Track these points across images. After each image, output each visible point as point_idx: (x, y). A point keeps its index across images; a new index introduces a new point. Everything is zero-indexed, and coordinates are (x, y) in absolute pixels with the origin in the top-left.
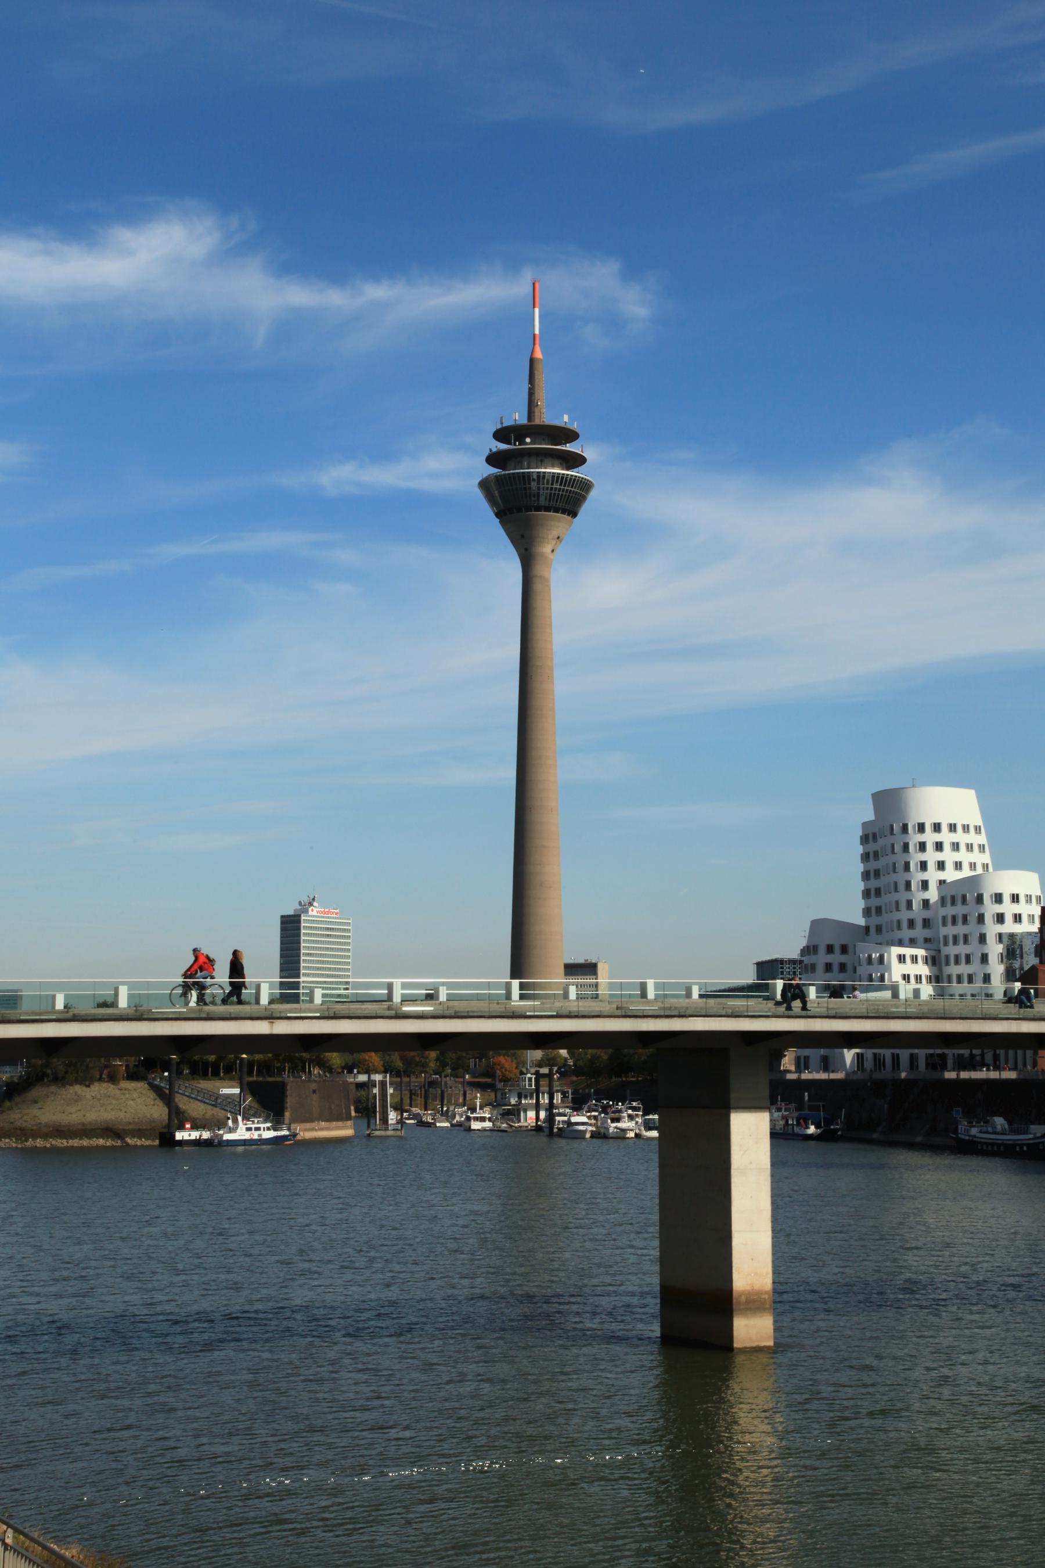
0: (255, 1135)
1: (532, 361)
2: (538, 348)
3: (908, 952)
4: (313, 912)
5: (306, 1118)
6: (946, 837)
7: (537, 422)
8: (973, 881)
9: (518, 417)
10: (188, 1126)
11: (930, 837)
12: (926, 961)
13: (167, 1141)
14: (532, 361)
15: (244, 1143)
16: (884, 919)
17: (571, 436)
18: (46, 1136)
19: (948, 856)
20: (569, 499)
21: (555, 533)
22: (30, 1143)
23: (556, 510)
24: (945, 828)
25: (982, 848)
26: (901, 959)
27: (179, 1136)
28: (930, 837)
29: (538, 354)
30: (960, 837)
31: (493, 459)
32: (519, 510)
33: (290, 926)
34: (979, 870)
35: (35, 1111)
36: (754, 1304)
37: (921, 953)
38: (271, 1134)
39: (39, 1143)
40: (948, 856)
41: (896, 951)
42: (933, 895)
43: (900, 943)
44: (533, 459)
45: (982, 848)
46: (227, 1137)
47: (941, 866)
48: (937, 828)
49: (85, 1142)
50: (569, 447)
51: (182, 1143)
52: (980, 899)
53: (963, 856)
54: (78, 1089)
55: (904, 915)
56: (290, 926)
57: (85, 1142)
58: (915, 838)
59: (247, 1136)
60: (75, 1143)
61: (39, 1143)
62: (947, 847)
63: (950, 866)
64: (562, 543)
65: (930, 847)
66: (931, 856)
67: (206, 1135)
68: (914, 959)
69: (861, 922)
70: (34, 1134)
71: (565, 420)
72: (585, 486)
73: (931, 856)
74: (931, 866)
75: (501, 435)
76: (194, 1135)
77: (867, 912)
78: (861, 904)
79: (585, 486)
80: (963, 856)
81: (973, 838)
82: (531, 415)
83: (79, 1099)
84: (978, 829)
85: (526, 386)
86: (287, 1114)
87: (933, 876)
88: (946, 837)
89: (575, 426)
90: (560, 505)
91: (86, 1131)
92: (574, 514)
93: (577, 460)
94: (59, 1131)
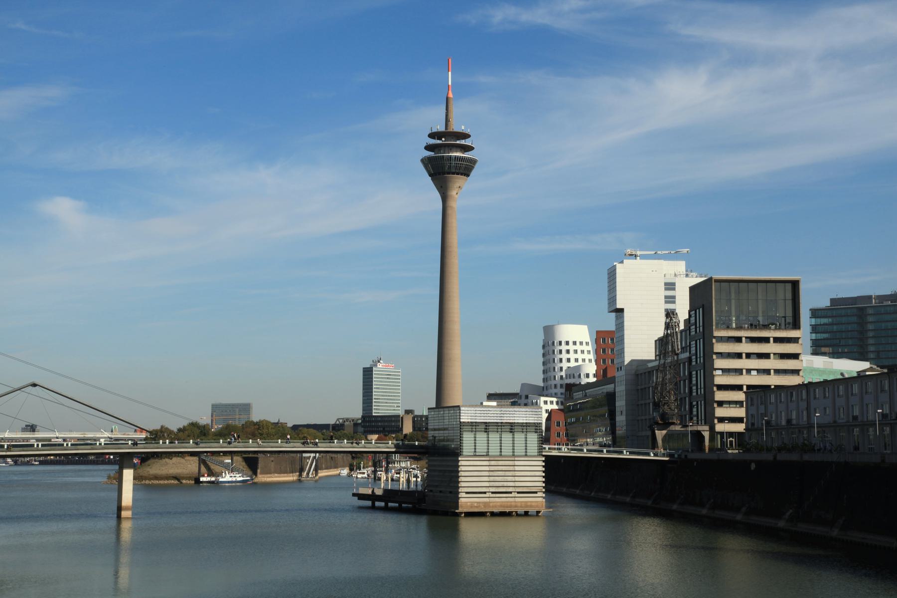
0: (234, 479)
1: (447, 98)
2: (450, 92)
3: (549, 399)
4: (380, 366)
5: (267, 472)
6: (571, 347)
7: (450, 130)
8: (578, 368)
9: (441, 128)
10: (753, 466)
11: (564, 347)
12: (557, 403)
13: (197, 481)
14: (447, 98)
15: (229, 482)
16: (549, 383)
17: (466, 136)
18: (150, 479)
19: (572, 356)
20: (466, 168)
21: (457, 185)
22: (143, 482)
23: (458, 174)
24: (578, 343)
25: (589, 352)
26: (546, 402)
27: (202, 479)
28: (564, 347)
29: (451, 95)
30: (578, 347)
31: (429, 148)
32: (439, 174)
33: (368, 373)
34: (580, 362)
35: (148, 469)
36: (127, 509)
37: (555, 400)
38: (241, 479)
39: (147, 482)
40: (572, 356)
41: (543, 399)
42: (563, 374)
43: (547, 396)
44: (447, 149)
45: (589, 352)
46: (221, 480)
47: (569, 360)
48: (575, 343)
49: (166, 482)
50: (463, 142)
51: (202, 482)
52: (580, 376)
53: (580, 356)
54: (167, 460)
55: (553, 383)
56: (368, 373)
57: (166, 482)
58: (558, 348)
59: (230, 479)
60: (162, 482)
61: (147, 482)
62: (579, 352)
63: (572, 360)
64: (463, 190)
65: (564, 352)
66: (564, 356)
67: (213, 479)
68: (552, 403)
69: (542, 384)
70: (146, 478)
71: (462, 128)
72: (473, 162)
73: (564, 356)
74: (564, 360)
75: (432, 135)
76: (209, 479)
77: (545, 380)
78: (542, 376)
79: (473, 162)
80: (580, 356)
81: (585, 348)
82: (446, 128)
83: (167, 464)
84: (587, 344)
85: (445, 111)
86: (259, 471)
87: (565, 365)
88: (571, 347)
89: (468, 131)
90: (461, 171)
91: (168, 477)
92: (468, 176)
93: (468, 149)
94: (156, 477)
